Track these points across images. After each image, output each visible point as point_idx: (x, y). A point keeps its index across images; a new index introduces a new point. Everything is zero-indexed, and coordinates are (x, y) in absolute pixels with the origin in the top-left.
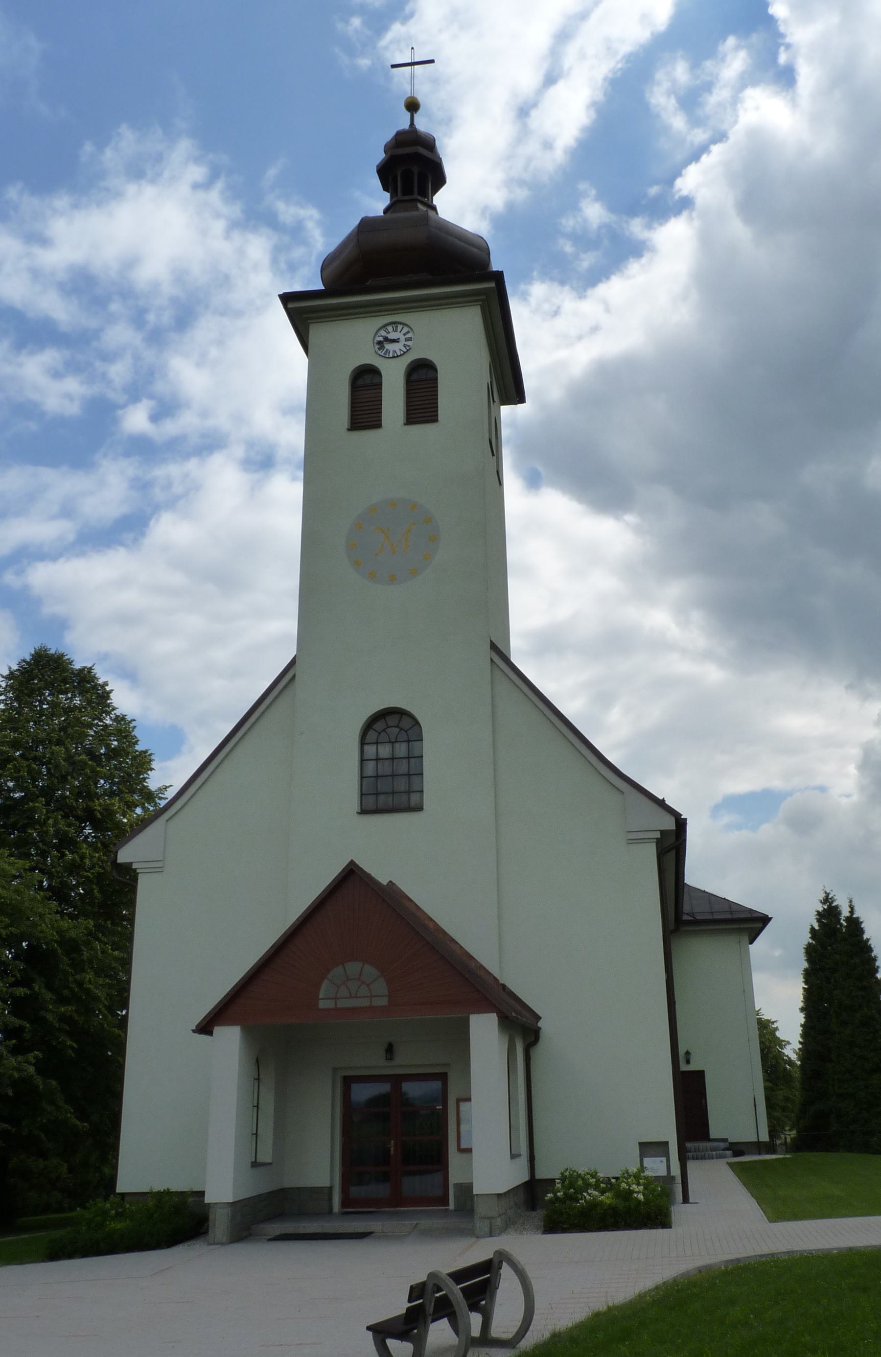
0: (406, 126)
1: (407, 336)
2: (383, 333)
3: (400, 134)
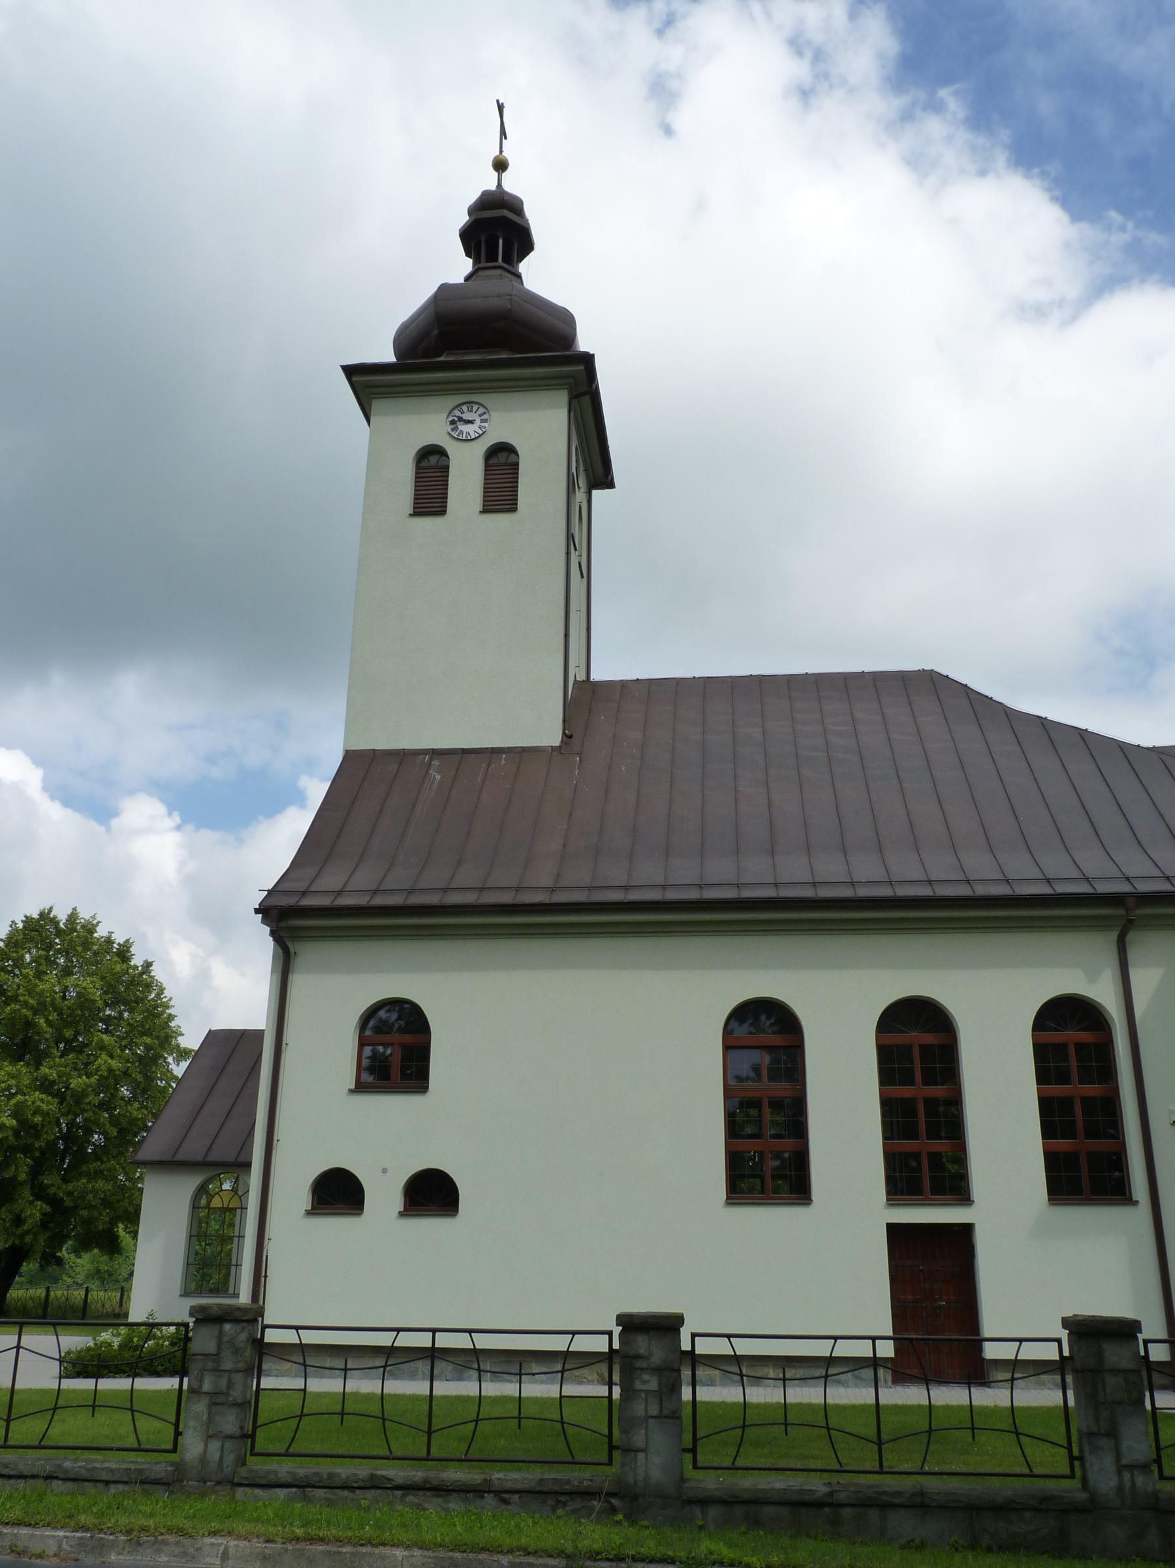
0: (493, 187)
1: (484, 417)
2: (457, 413)
3: (485, 194)
